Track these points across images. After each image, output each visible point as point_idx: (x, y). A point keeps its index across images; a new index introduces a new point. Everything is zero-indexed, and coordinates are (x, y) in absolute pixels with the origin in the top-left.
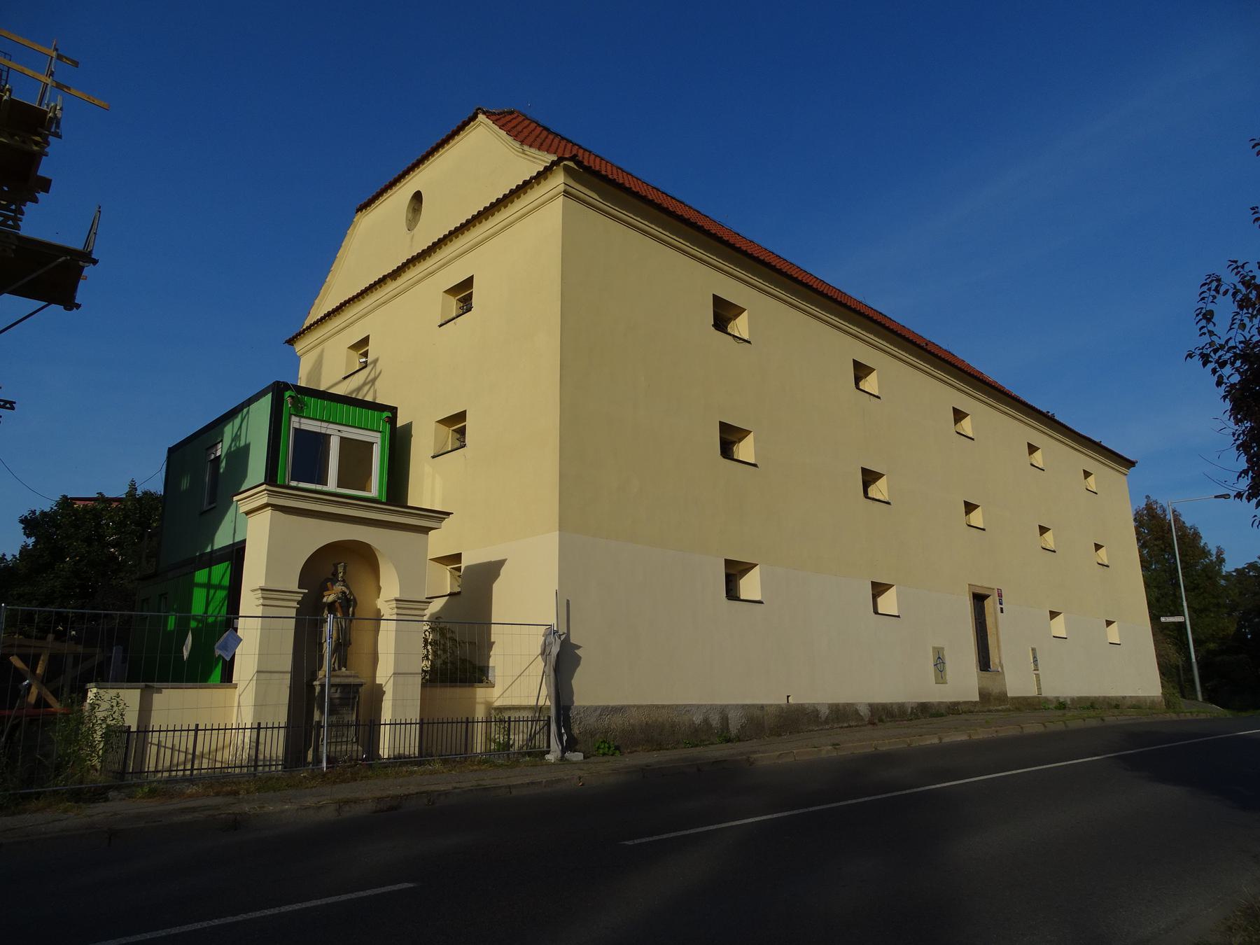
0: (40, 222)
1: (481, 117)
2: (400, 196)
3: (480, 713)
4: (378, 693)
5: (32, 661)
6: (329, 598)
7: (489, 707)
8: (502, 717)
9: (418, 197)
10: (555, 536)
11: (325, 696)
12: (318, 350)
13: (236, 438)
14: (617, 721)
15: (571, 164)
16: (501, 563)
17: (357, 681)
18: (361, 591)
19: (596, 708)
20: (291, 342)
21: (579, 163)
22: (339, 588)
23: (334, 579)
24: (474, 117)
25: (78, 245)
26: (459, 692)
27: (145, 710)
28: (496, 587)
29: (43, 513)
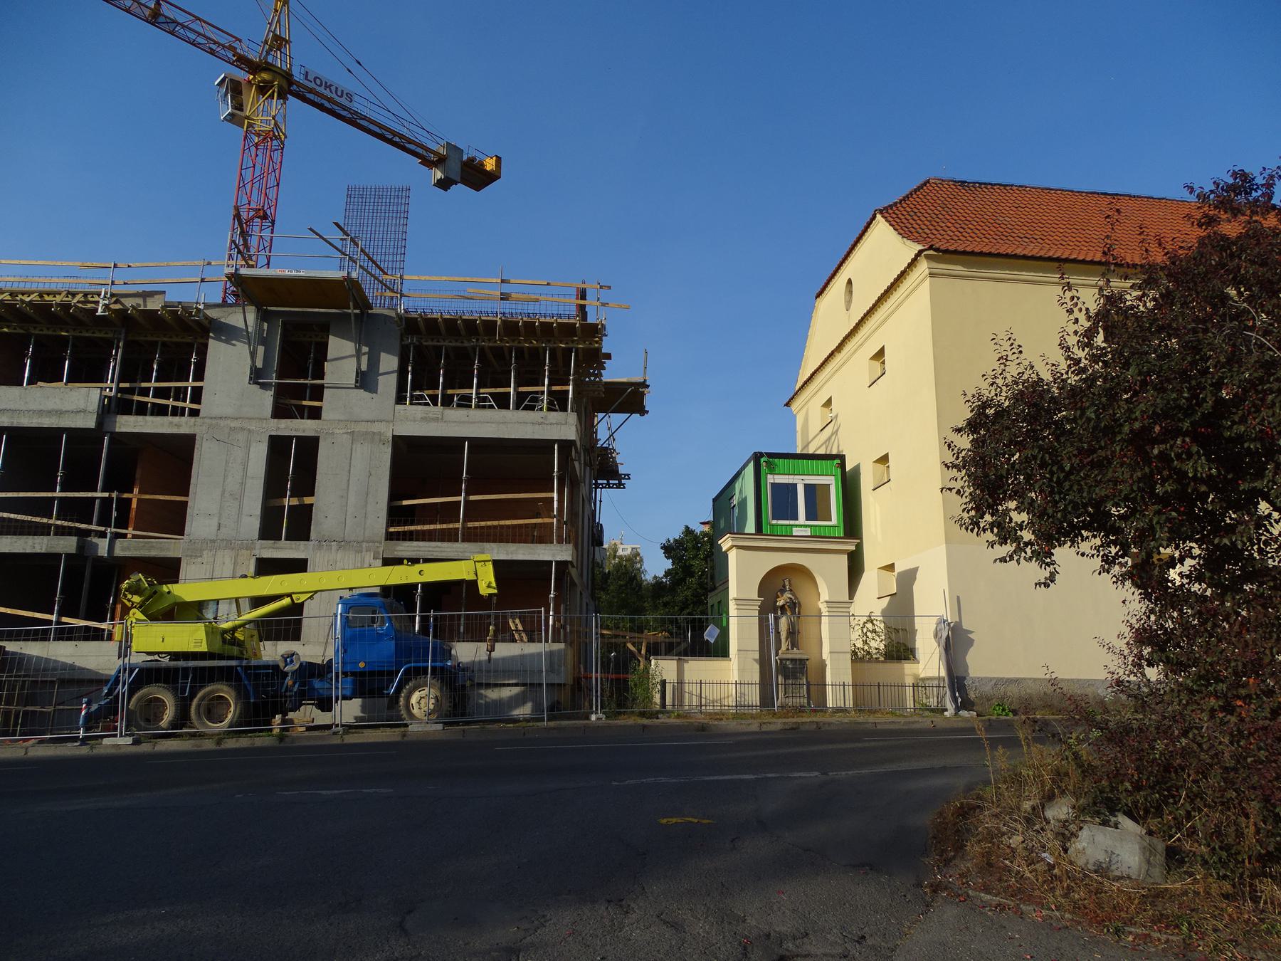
0: (613, 373)
1: (879, 216)
2: (839, 284)
3: (909, 681)
4: (823, 666)
5: (638, 645)
6: (780, 603)
7: (916, 677)
8: (920, 684)
9: (850, 282)
10: (942, 548)
11: (788, 669)
12: (804, 410)
13: (741, 492)
14: (1013, 690)
15: (931, 252)
16: (916, 570)
17: (804, 657)
18: (804, 597)
19: (991, 679)
20: (788, 404)
21: (937, 250)
22: (787, 595)
23: (783, 591)
24: (874, 217)
25: (639, 379)
26: (893, 666)
27: (680, 672)
28: (916, 587)
29: (676, 540)
